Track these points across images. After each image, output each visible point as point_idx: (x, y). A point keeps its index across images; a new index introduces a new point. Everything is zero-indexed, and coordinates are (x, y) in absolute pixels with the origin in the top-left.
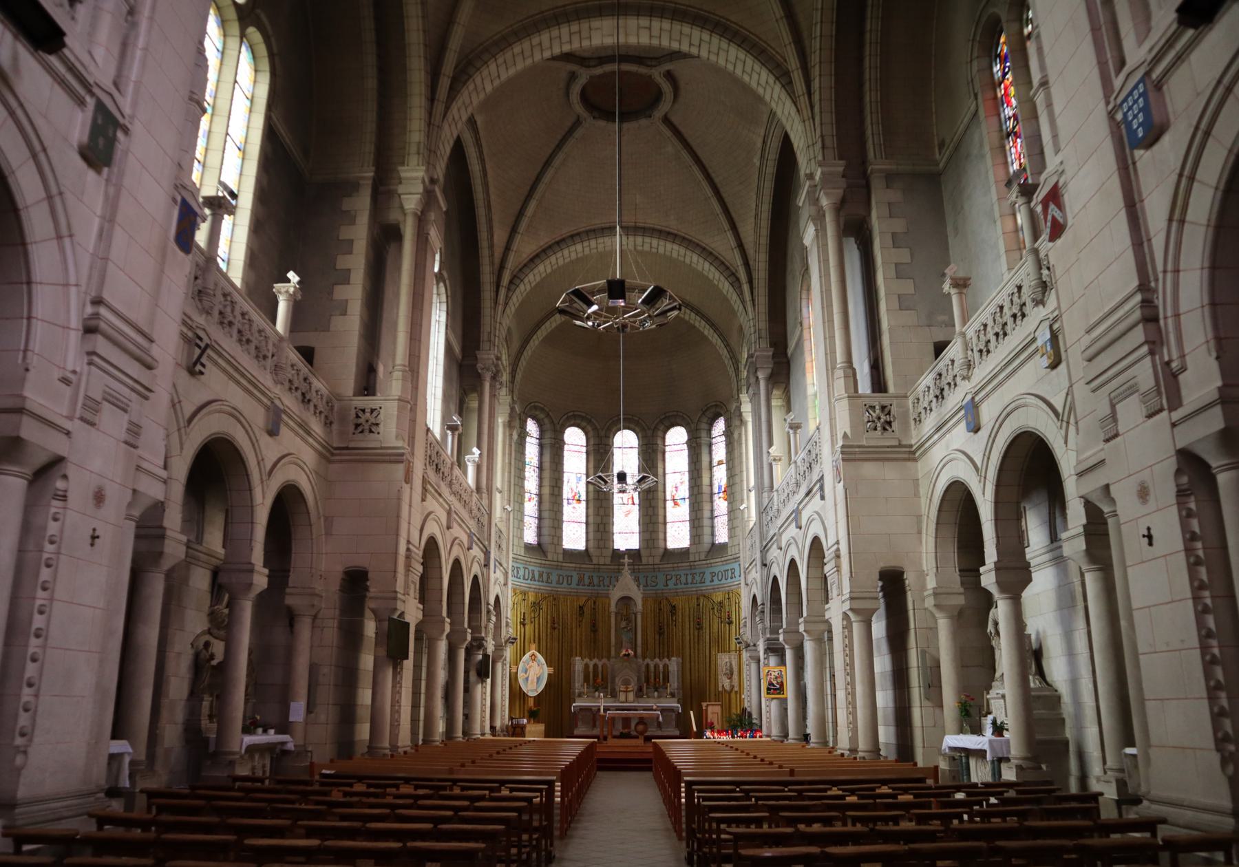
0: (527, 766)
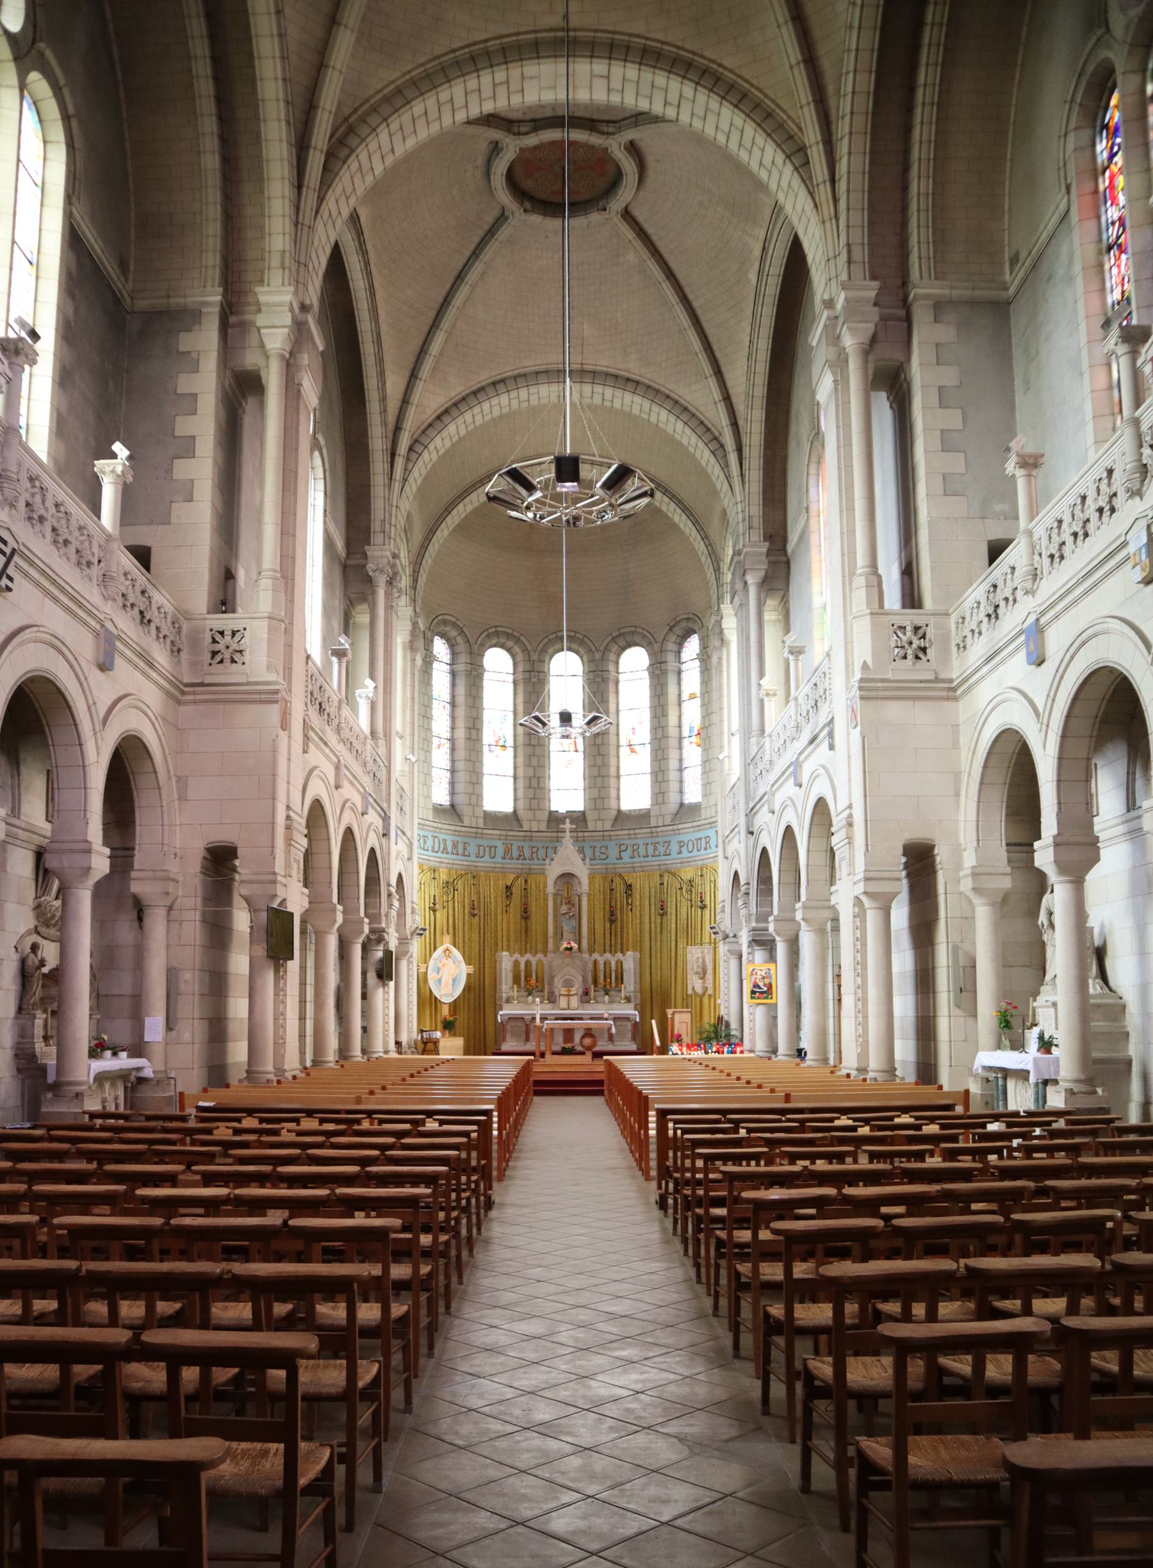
0: (441, 1092)
